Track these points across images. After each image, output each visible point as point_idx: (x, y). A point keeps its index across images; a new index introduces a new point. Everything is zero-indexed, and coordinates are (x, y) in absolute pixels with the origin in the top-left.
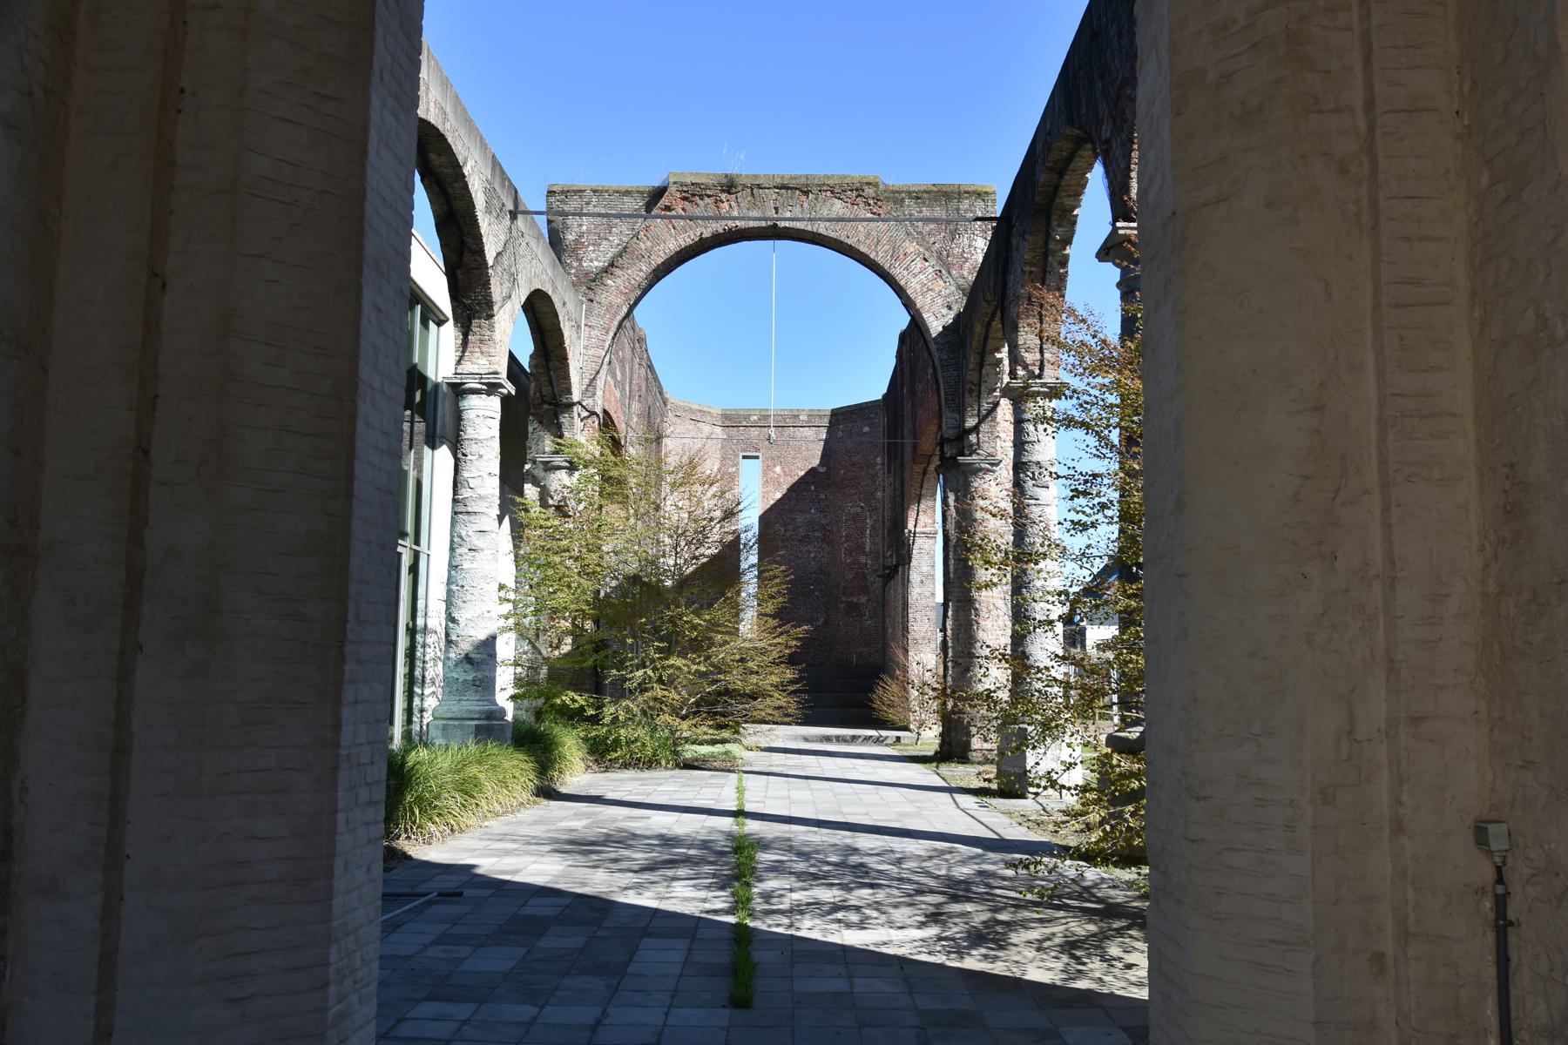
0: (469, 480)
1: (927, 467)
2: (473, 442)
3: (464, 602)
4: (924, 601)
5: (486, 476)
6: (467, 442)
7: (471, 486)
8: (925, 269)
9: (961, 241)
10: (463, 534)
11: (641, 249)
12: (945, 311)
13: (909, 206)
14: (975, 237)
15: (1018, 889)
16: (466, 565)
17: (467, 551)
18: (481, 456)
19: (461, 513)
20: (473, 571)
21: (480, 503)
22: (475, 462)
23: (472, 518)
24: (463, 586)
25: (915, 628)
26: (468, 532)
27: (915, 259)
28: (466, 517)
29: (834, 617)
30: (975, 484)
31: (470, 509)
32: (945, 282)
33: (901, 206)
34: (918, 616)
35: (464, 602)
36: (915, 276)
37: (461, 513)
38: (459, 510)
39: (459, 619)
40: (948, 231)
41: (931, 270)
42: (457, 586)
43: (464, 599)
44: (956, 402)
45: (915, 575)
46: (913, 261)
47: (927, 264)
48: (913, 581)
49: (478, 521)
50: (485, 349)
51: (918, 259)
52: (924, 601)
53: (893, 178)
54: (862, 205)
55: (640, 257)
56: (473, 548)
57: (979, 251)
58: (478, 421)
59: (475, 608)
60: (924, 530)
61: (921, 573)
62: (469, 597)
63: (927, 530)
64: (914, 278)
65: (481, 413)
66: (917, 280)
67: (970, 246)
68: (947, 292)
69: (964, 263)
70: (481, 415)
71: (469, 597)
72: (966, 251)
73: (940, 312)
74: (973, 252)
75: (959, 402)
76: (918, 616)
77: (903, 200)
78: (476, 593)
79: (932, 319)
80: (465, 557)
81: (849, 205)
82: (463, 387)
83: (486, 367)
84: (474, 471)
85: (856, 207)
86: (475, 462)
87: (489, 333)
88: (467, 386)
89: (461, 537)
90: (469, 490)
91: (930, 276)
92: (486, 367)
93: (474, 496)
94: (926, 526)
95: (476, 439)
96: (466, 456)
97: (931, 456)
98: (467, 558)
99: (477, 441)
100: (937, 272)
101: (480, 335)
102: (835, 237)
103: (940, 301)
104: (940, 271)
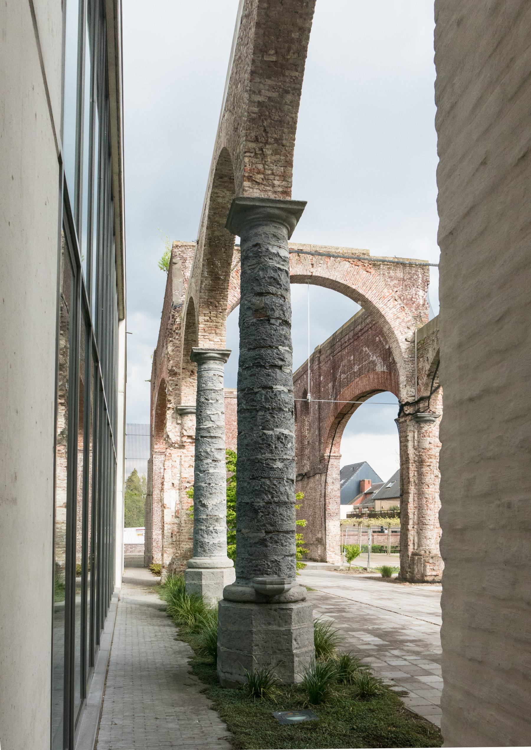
0: (211, 416)
1: (341, 420)
2: (213, 391)
3: (211, 494)
4: (334, 493)
5: (220, 414)
6: (208, 391)
7: (212, 419)
8: (396, 306)
9: (411, 291)
10: (208, 450)
11: (234, 283)
12: (406, 330)
13: (383, 269)
14: (419, 289)
15: (404, 657)
16: (211, 471)
17: (211, 461)
18: (217, 400)
19: (206, 437)
20: (216, 474)
21: (218, 430)
22: (214, 405)
23: (214, 440)
24: (210, 484)
25: (329, 507)
26: (211, 449)
27: (390, 300)
28: (210, 440)
29: (426, 508)
30: (425, 429)
31: (212, 435)
32: (406, 314)
33: (378, 269)
34: (331, 501)
35: (211, 494)
36: (390, 309)
37: (206, 437)
38: (205, 435)
39: (208, 504)
40: (404, 285)
41: (399, 306)
42: (205, 483)
43: (211, 492)
44: (413, 382)
45: (329, 478)
46: (389, 301)
47: (396, 303)
48: (328, 482)
49: (217, 442)
50: (218, 331)
51: (392, 300)
52: (334, 493)
53: (376, 253)
54: (361, 266)
55: (234, 288)
56: (215, 459)
57: (421, 297)
58: (214, 378)
59: (218, 497)
60: (334, 454)
61: (333, 478)
62: (214, 491)
63: (336, 454)
64: (390, 310)
65: (216, 373)
66: (391, 311)
67: (416, 294)
68: (408, 319)
69: (413, 303)
70: (216, 374)
71: (214, 491)
72: (414, 297)
73: (404, 331)
74: (417, 298)
75: (415, 382)
76: (331, 501)
77: (379, 265)
78: (218, 488)
79: (400, 334)
80: (210, 465)
81: (354, 266)
82: (205, 355)
83: (219, 343)
84: (213, 410)
85: (357, 267)
86: (214, 405)
87: (221, 321)
88: (208, 355)
89: (207, 453)
90: (211, 422)
91: (398, 310)
92: (219, 343)
93: (215, 426)
94: (335, 453)
95: (214, 390)
96: (209, 400)
97: (345, 414)
98: (212, 466)
99: (215, 391)
100: (402, 308)
101: (216, 322)
102: (346, 284)
103: (403, 324)
104: (404, 307)
